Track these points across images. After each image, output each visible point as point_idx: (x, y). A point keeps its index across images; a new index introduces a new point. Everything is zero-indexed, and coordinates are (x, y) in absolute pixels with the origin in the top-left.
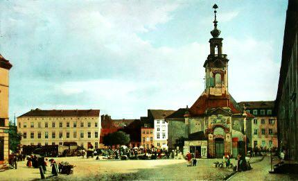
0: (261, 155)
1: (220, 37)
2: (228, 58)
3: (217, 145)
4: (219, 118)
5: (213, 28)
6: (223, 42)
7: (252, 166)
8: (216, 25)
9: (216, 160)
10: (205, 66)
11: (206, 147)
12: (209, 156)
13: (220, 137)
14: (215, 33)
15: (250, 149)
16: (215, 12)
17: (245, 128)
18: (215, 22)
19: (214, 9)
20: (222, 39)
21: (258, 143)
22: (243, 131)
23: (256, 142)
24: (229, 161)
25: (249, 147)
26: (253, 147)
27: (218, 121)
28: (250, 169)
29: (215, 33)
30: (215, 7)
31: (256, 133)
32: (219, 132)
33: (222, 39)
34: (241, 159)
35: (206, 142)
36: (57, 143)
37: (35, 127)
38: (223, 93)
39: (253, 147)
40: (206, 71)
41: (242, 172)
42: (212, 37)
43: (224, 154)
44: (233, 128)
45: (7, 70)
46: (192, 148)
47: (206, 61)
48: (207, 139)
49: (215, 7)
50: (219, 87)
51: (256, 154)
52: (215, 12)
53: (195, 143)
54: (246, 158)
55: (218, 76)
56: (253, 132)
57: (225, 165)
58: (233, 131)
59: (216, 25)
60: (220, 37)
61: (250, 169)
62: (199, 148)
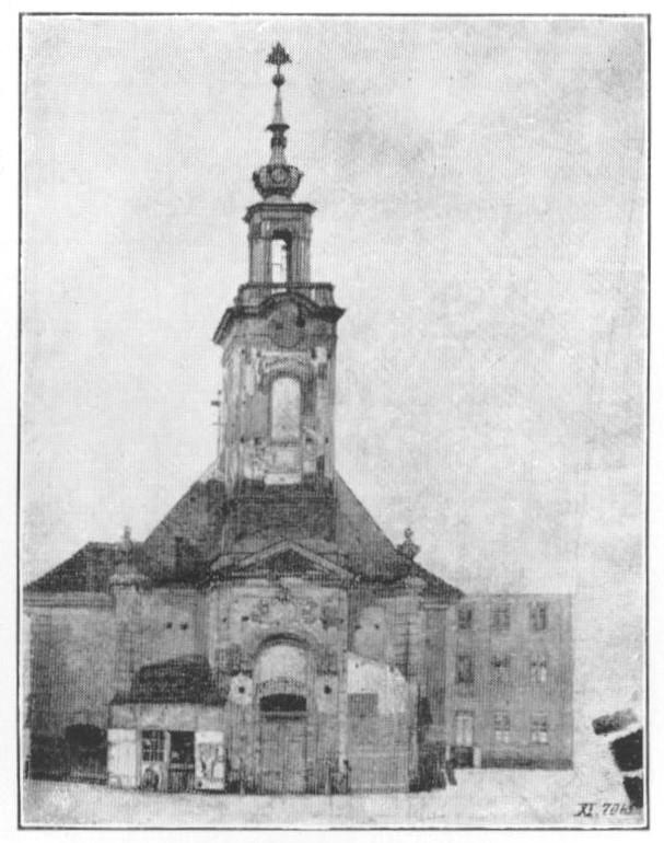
1: (298, 197)
2: (340, 300)
4: (284, 597)
5: (263, 155)
6: (316, 221)
8: (278, 142)
10: (219, 338)
14: (276, 183)
16: (278, 81)
18: (278, 131)
19: (272, 70)
20: (308, 209)
27: (278, 612)
29: (276, 183)
30: (279, 56)
32: (280, 666)
33: (308, 209)
38: (309, 467)
40: (226, 361)
42: (257, 198)
45: (212, 336)
46: (151, 743)
47: (229, 311)
49: (279, 56)
50: (591, 809)
52: (278, 81)
53: (172, 717)
55: (286, 392)
59: (278, 142)
60: (298, 197)
62: (183, 742)
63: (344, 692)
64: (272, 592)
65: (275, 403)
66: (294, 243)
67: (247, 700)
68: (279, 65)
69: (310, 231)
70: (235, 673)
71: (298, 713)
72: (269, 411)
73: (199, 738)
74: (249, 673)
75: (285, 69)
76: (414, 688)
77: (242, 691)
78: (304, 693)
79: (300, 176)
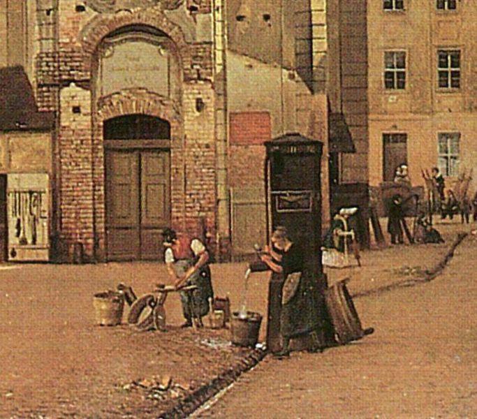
0: (433, 237)
3: (125, 163)
7: (368, 313)
9: (114, 274)
11: (42, 182)
12: (61, 250)
13: (144, 105)
15: (356, 192)
17: (321, 45)
21: (414, 147)
22: (306, 71)
23: (393, 139)
24: (205, 277)
25: (347, 176)
26: (375, 178)
28: (356, 333)
31: (394, 81)
34: (291, 261)
35: (42, 141)
36: (172, 146)
37: (83, 110)
39: (375, 178)
41: (301, 358)
43: (170, 235)
44: (232, 45)
48: (49, 124)
51: (395, 228)
54: (328, 258)
56: (376, 74)
57: (175, 314)
58: (237, 64)
61: (356, 333)
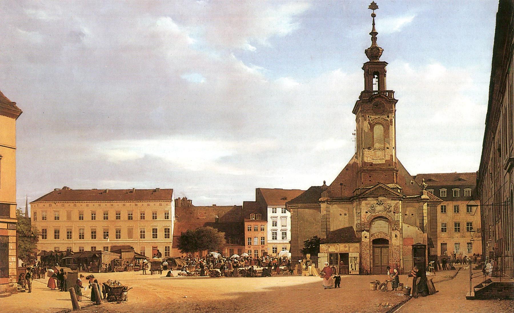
1: (381, 59)
5: (369, 44)
6: (387, 68)
16: (374, 16)
19: (371, 11)
27: (379, 208)
60: (381, 59)
62: (344, 256)
63: (377, 78)
64: (376, 202)
65: (375, 136)
66: (380, 76)
67: (367, 240)
68: (374, 10)
69: (9, 100)
70: (363, 231)
71: (386, 245)
72: (373, 137)
73: (350, 255)
74: (368, 231)
75: (376, 12)
76: (426, 235)
77: (366, 237)
78: (388, 238)
79: (383, 50)
